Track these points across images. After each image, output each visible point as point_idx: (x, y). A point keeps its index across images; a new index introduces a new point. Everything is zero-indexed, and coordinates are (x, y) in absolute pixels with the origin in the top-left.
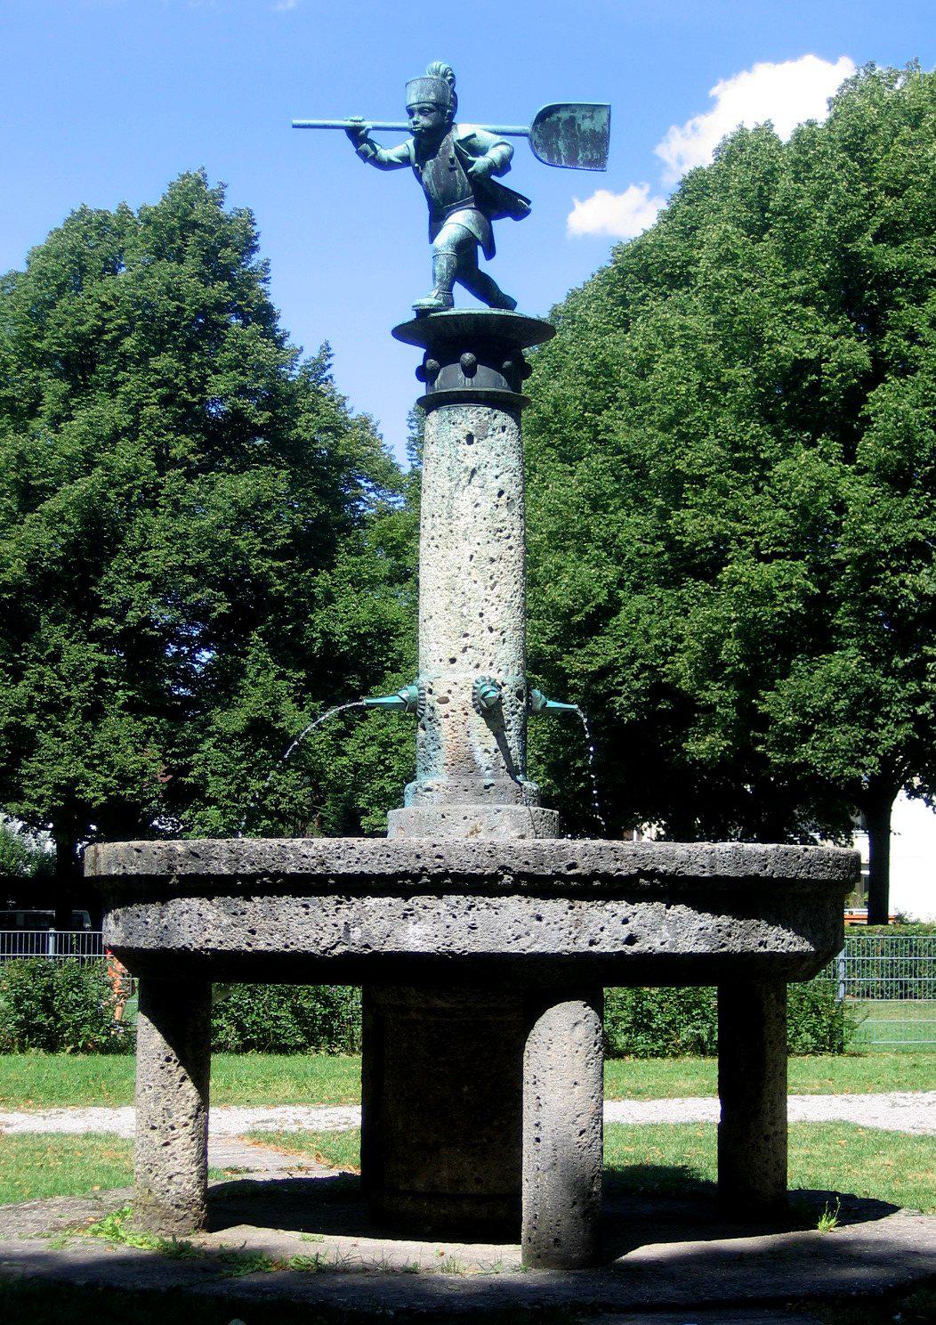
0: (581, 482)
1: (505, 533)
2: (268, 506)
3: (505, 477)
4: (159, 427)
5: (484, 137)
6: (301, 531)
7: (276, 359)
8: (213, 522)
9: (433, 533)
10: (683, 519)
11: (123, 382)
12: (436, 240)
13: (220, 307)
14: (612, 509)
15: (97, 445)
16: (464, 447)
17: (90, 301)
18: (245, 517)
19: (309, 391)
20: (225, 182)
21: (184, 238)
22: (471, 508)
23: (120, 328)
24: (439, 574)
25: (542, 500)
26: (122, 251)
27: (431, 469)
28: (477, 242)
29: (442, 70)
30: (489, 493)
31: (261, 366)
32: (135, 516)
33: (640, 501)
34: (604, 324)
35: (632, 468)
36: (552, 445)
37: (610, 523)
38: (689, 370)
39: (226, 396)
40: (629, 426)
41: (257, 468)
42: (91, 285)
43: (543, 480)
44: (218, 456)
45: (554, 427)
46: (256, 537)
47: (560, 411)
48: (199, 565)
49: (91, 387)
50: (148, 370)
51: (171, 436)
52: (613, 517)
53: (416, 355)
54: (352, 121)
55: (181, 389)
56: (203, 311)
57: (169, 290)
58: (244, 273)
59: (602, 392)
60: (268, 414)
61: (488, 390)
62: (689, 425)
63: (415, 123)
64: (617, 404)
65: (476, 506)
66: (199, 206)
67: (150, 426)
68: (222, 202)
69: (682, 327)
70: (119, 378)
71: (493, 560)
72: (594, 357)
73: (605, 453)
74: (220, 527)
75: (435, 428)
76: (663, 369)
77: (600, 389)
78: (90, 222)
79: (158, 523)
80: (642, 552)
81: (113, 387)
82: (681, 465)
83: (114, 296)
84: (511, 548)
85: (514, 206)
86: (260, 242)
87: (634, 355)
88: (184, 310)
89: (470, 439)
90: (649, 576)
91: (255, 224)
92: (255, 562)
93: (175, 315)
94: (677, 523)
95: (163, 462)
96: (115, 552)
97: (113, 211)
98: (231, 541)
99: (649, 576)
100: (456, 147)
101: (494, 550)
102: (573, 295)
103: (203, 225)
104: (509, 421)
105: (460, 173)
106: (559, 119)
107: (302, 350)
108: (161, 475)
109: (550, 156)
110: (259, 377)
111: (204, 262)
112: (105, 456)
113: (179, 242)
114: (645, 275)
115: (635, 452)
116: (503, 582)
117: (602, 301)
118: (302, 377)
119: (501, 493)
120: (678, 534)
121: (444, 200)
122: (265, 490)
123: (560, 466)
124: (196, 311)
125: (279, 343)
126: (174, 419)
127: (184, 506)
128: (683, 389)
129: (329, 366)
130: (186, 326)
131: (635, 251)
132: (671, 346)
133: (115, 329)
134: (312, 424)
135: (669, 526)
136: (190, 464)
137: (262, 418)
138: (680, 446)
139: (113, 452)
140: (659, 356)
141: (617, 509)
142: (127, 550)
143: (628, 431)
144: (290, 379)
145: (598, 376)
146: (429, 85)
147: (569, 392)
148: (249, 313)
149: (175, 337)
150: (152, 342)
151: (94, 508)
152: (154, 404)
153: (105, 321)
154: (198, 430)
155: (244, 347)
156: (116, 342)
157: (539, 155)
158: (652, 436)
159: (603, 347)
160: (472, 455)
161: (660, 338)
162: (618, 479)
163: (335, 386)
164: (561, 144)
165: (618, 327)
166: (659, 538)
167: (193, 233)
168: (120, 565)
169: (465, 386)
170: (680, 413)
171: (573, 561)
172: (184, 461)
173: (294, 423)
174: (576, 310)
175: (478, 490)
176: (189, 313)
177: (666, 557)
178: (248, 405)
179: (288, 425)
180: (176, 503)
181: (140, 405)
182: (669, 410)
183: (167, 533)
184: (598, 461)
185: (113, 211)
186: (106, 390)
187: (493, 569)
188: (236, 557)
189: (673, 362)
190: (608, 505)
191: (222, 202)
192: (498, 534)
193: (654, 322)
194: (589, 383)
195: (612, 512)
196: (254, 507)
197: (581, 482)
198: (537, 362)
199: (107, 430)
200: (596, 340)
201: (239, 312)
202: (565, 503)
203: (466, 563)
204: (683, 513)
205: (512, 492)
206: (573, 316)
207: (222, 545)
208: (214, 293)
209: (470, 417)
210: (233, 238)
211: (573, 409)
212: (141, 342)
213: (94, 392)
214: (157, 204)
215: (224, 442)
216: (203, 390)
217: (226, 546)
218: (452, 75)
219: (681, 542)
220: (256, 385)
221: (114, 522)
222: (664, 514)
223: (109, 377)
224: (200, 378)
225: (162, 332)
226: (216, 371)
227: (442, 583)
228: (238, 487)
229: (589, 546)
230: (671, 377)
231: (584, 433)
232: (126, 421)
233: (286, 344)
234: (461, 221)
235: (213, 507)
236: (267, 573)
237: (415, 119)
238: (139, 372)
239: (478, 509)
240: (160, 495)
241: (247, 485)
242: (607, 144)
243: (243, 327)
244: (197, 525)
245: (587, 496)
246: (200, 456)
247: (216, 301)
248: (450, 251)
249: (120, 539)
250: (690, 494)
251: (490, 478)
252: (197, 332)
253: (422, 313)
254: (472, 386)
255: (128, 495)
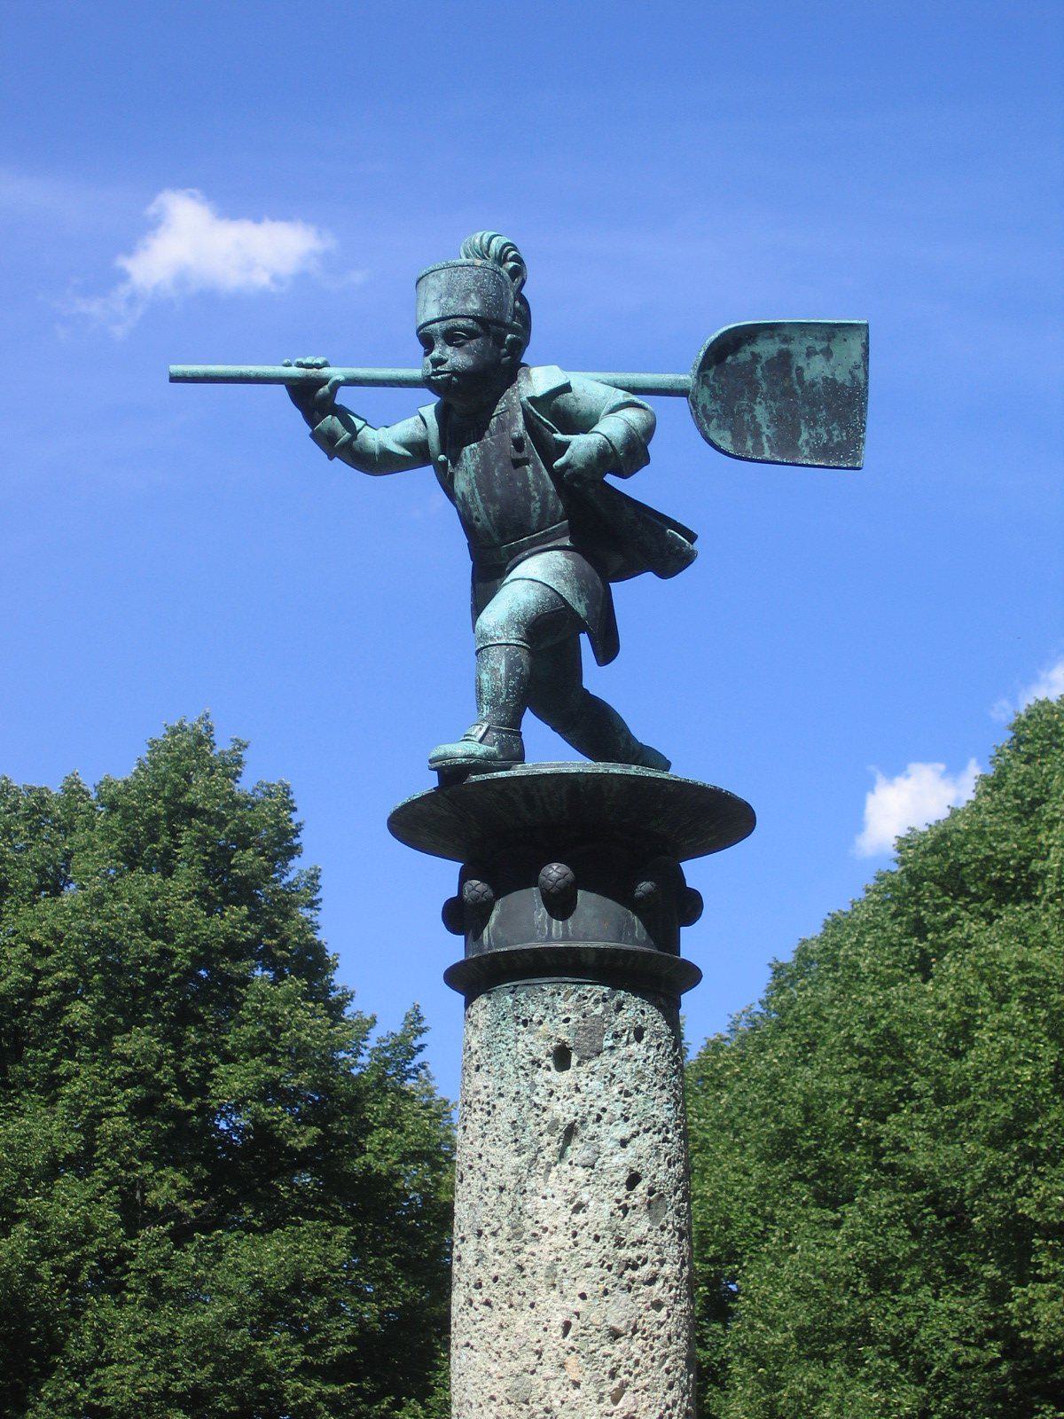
0: (851, 1240)
1: (644, 1271)
2: (316, 1289)
3: (644, 1143)
4: (130, 1153)
5: (591, 389)
6: (373, 1332)
7: (330, 1036)
8: (219, 1317)
9: (479, 1272)
10: (1033, 1302)
11: (68, 1078)
12: (484, 616)
13: (235, 950)
14: (906, 1285)
15: (21, 1184)
16: (548, 1075)
17: (13, 940)
18: (276, 1307)
19: (385, 1091)
20: (244, 739)
21: (174, 834)
22: (565, 1214)
23: (65, 986)
24: (493, 1368)
25: (785, 1272)
26: (68, 856)
27: (474, 1127)
28: (579, 625)
29: (496, 245)
30: (606, 1179)
31: (304, 1049)
32: (86, 1306)
33: (956, 1271)
34: (888, 967)
35: (941, 1216)
36: (801, 1178)
37: (904, 1311)
38: (1038, 1040)
39: (243, 1100)
40: (936, 1137)
41: (298, 1224)
42: (15, 913)
43: (788, 1238)
44: (232, 1205)
45: (805, 1144)
46: (294, 1343)
47: (814, 1118)
48: (195, 1390)
49: (13, 1086)
50: (110, 1058)
51: (149, 1169)
52: (910, 1300)
53: (441, 877)
54: (300, 365)
55: (167, 1088)
56: (206, 955)
57: (147, 921)
58: (275, 892)
59: (887, 1084)
60: (314, 1131)
61: (601, 945)
62: (1038, 1136)
63: (438, 362)
64: (913, 1104)
65: (576, 1210)
66: (199, 780)
67: (113, 1152)
68: (238, 773)
69: (1023, 966)
70: (62, 1070)
71: (615, 1335)
72: (871, 1023)
73: (894, 1187)
74: (231, 1325)
75: (485, 1035)
76: (992, 1039)
77: (882, 1078)
78: (15, 808)
79: (122, 1319)
80: (960, 1361)
81: (51, 1086)
82: (1027, 1208)
83: (53, 930)
84: (658, 1305)
85: (656, 546)
86: (303, 839)
87: (940, 1015)
88: (173, 955)
89: (562, 1057)
90: (974, 1404)
91: (294, 809)
92: (292, 1385)
93: (157, 963)
94: (1022, 1308)
95: (134, 1214)
96: (48, 1370)
97: (56, 790)
98: (251, 1350)
99: (974, 1404)
100: (526, 413)
101: (618, 1311)
102: (835, 923)
103: (204, 811)
104: (652, 1018)
105: (537, 471)
106: (756, 357)
107: (374, 1021)
108: (131, 1235)
109: (738, 437)
110: (300, 1068)
111: (206, 874)
112: (35, 1204)
113: (165, 839)
114: (953, 883)
115: (945, 1184)
116: (639, 1383)
117: (884, 930)
118: (373, 1067)
119: (633, 1180)
120: (1025, 1327)
121: (502, 534)
122: (311, 1261)
123: (815, 1214)
124: (192, 956)
125: (336, 1010)
126: (156, 1140)
127: (170, 1289)
128: (1027, 1073)
129: (421, 1048)
130: (176, 983)
131: (935, 843)
132: (1004, 1000)
133: (55, 988)
134: (390, 1147)
135: (1009, 1313)
136: (181, 1216)
137: (304, 1139)
138: (1024, 1172)
139: (48, 1197)
140: (984, 1017)
141: (915, 1287)
142: (70, 1365)
143: (933, 1149)
144: (355, 1071)
145: (879, 1056)
146: (466, 279)
147: (831, 1085)
148: (285, 960)
149: (156, 999)
150: (120, 1010)
151: (14, 1293)
152: (121, 1114)
153: (39, 975)
154: (196, 1159)
155: (274, 1017)
156: (57, 1010)
157: (713, 436)
158: (974, 1158)
159: (887, 1006)
160: (567, 1094)
161: (985, 985)
162: (916, 1233)
163: (433, 1084)
164: (761, 413)
165: (912, 972)
166: (992, 1335)
167: (189, 825)
168: (57, 1392)
169: (549, 938)
170: (1024, 1116)
171: (840, 1379)
172: (170, 1212)
173: (360, 1146)
174: (838, 946)
175: (580, 1174)
176: (182, 960)
177: (1004, 1369)
178: (280, 1117)
179: (351, 1148)
180: (155, 1284)
181: (97, 1117)
182: (1002, 1110)
183: (139, 1336)
184: (880, 1202)
185: (56, 790)
186: (39, 1091)
187: (617, 1355)
188: (259, 1377)
189: (1008, 1027)
190: (901, 1279)
191: (238, 773)
192: (629, 1273)
193: (973, 959)
194: (864, 1068)
195: (907, 1292)
196: (295, 1288)
197: (851, 1240)
198: (774, 1036)
199: (38, 1159)
200: (873, 994)
201: (268, 959)
202: (824, 1277)
203: (554, 1342)
204: (1032, 1290)
205: (661, 1177)
206: (835, 957)
207: (235, 1356)
208: (225, 925)
209: (561, 1009)
210: (257, 832)
211: (837, 1114)
212: (99, 1008)
213: (18, 1095)
214: (128, 776)
215: (243, 1180)
216: (204, 1091)
217: (243, 1358)
218: (517, 259)
219: (1031, 1343)
220: (295, 1083)
221: (47, 1318)
222: (999, 1294)
223: (45, 1069)
224: (199, 1070)
225: (136, 991)
226: (228, 1058)
227: (499, 1389)
228: (262, 1256)
229: (869, 1352)
230: (1006, 1054)
231: (858, 1156)
232: (72, 1144)
233: (348, 1011)
234: (538, 575)
235: (220, 1291)
236: (312, 1404)
237: (435, 354)
238: (95, 1059)
239: (580, 1218)
240: (127, 1271)
241: (278, 1253)
242: (863, 411)
243: (274, 983)
244: (192, 1322)
245: (864, 1265)
246: (198, 1204)
247: (227, 939)
248: (513, 637)
249: (58, 1347)
250: (1043, 1258)
251: (608, 1145)
252: (193, 994)
253: (452, 774)
254: (565, 938)
255: (74, 1271)
